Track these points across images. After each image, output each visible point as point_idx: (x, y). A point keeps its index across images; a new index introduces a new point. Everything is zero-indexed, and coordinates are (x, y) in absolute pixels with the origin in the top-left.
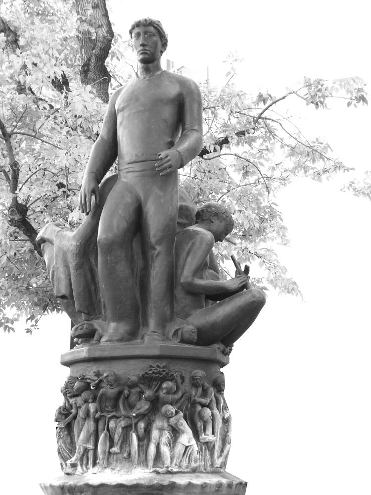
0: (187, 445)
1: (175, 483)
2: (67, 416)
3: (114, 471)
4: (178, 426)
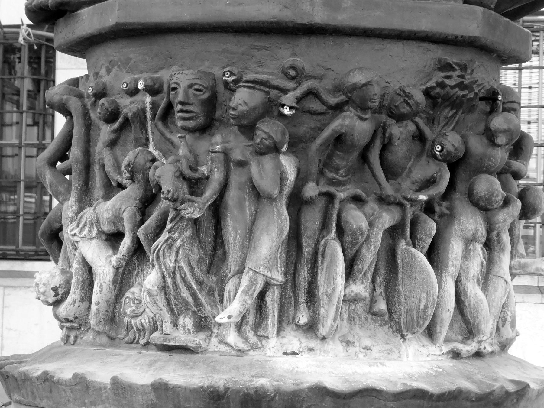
3: (351, 350)
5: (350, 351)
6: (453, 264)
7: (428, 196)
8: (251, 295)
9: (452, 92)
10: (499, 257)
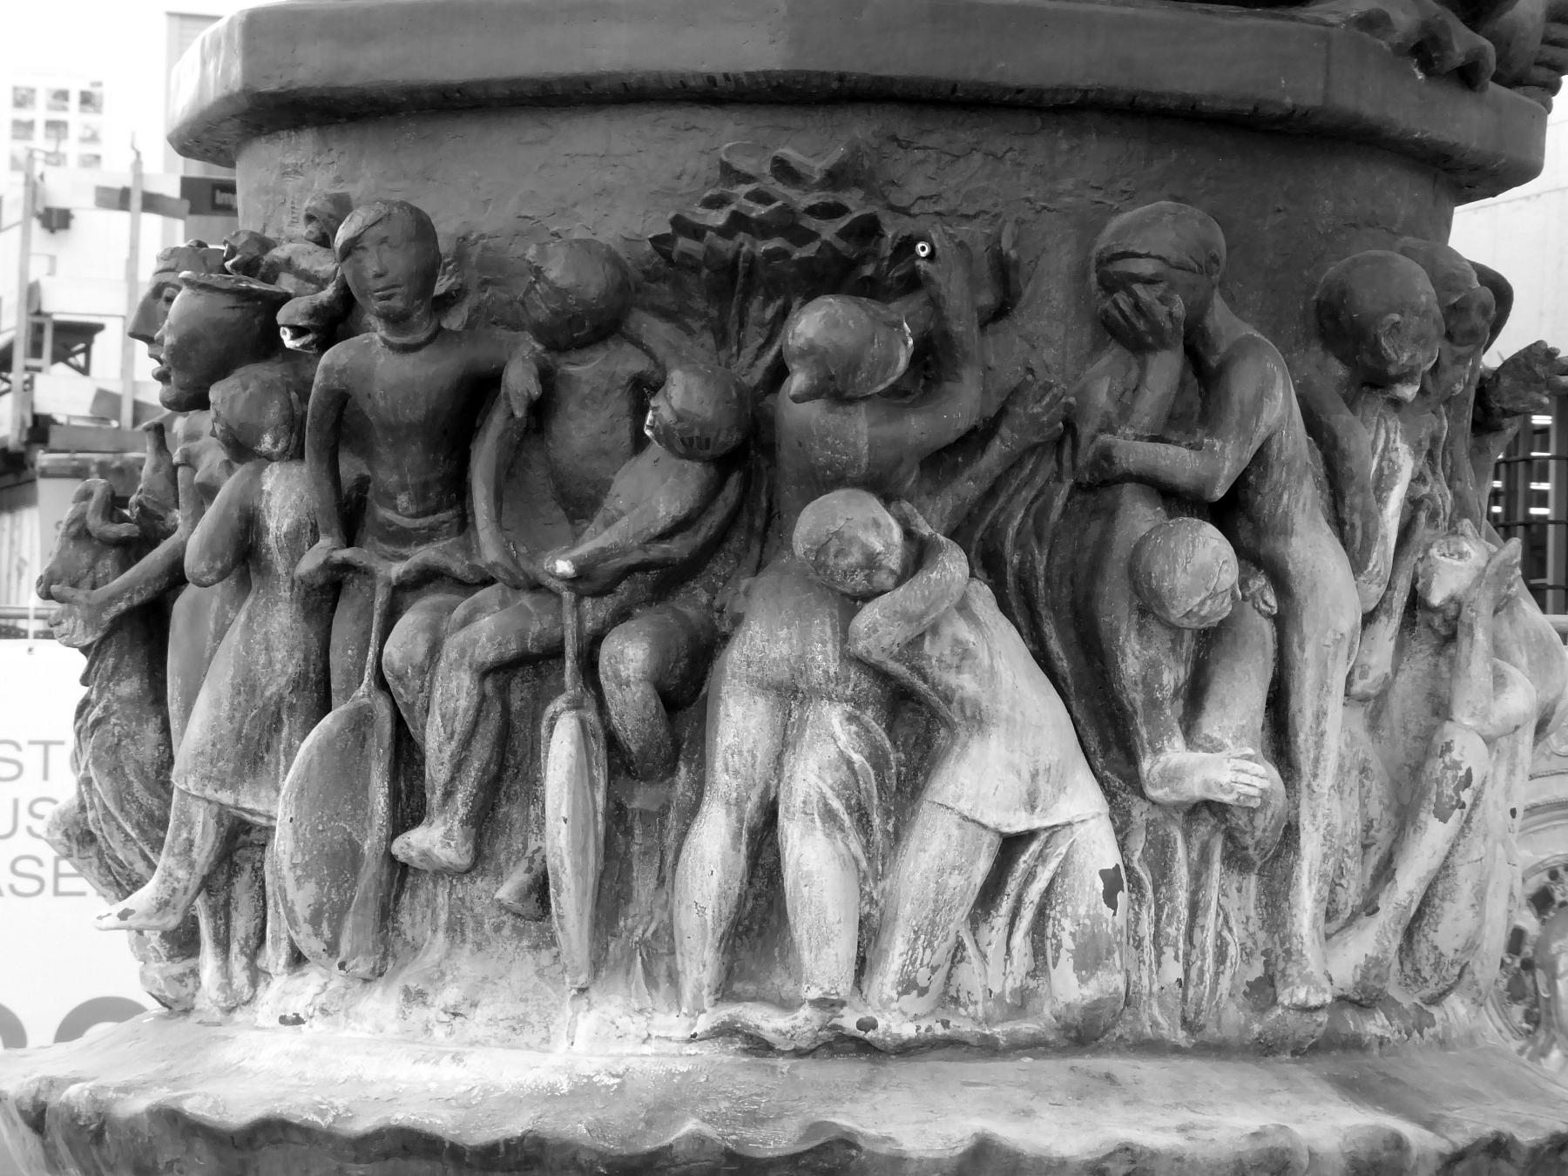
0: (1019, 823)
1: (847, 1141)
2: (131, 550)
3: (418, 1014)
4: (934, 670)
5: (413, 1018)
6: (726, 765)
7: (574, 561)
8: (180, 854)
9: (725, 246)
10: (965, 745)
